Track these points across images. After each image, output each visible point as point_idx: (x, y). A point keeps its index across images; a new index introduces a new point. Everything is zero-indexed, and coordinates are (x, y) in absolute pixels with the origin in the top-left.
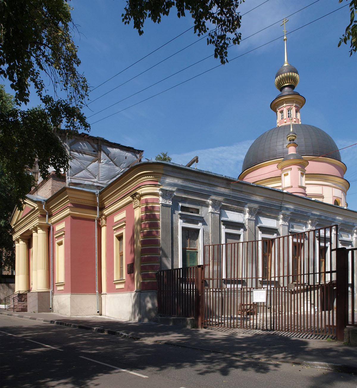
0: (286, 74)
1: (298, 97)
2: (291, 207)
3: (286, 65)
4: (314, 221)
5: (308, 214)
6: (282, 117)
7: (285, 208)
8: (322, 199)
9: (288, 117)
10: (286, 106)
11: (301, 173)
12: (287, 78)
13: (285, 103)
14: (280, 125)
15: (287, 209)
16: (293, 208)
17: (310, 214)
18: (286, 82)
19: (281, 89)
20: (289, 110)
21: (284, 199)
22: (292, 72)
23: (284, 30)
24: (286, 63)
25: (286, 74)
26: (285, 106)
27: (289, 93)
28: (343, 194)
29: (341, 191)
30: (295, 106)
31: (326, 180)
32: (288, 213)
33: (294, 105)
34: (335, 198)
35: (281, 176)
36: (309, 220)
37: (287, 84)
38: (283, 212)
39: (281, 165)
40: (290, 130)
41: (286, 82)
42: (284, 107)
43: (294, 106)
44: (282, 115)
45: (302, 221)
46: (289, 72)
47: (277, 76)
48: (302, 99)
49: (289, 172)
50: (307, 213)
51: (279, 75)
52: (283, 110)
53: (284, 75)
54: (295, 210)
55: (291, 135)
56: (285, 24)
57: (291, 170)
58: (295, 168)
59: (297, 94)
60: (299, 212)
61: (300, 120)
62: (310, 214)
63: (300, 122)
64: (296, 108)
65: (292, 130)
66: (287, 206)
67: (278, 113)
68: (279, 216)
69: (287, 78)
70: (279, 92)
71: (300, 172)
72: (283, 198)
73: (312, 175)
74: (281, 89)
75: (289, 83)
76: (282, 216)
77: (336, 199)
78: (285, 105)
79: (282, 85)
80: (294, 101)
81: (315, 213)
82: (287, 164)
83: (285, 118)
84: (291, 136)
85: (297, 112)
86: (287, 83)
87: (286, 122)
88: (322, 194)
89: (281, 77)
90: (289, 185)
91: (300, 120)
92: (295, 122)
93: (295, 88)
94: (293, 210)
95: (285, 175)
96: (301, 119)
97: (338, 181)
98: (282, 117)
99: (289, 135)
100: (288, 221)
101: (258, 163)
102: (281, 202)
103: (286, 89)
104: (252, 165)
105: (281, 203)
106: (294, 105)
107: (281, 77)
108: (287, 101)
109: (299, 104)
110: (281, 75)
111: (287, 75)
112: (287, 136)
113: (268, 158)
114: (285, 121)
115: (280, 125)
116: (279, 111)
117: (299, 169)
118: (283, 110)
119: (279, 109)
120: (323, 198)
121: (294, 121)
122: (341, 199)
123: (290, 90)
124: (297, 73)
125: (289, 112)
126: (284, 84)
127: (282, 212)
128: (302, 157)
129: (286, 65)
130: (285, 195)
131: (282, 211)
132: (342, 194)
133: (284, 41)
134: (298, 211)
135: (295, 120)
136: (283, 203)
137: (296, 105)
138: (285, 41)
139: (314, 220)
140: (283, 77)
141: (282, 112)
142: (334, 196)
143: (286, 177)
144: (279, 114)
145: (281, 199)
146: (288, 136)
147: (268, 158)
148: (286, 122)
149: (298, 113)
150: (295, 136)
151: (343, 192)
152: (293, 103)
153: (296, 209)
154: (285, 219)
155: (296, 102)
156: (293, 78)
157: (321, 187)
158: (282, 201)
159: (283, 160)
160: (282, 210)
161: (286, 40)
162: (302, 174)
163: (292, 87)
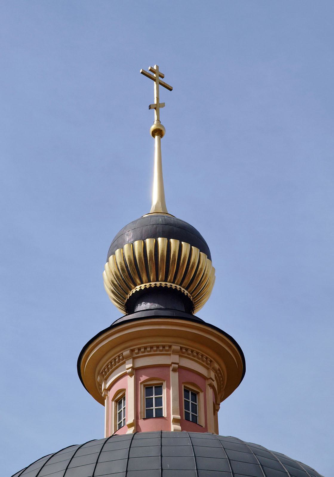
80: (170, 347)
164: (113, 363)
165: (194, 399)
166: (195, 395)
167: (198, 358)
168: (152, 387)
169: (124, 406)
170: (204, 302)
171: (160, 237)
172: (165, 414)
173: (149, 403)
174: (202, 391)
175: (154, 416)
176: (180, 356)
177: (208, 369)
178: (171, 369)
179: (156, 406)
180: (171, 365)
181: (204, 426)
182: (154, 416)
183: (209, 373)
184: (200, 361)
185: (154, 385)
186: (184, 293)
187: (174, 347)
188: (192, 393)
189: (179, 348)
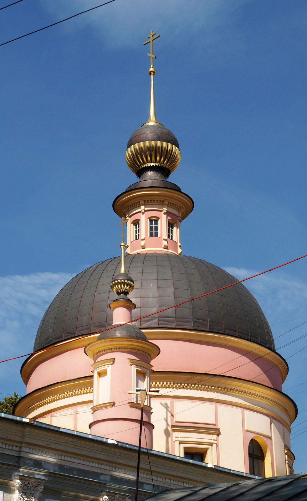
0: (147, 143)
1: (172, 194)
2: (51, 459)
3: (151, 124)
4: (118, 496)
5: (102, 477)
6: (136, 233)
7: (31, 463)
8: (215, 437)
9: (149, 235)
10: (146, 211)
11: (137, 371)
12: (150, 151)
13: (143, 205)
14: (132, 251)
15: (38, 464)
16: (55, 461)
17: (108, 478)
18: (149, 159)
19: (140, 172)
20: (154, 220)
21: (27, 440)
22: (167, 142)
23: (150, 53)
24: (152, 121)
25: (147, 143)
26: (143, 211)
27: (153, 183)
28: (274, 424)
29: (267, 419)
30: (167, 213)
31: (226, 390)
32: (40, 474)
33: (165, 209)
34: (251, 436)
35: (93, 376)
36: (103, 493)
37: (152, 164)
38: (23, 472)
39: (94, 348)
40: (120, 271)
41: (149, 159)
42: (140, 212)
43: (165, 213)
44: (136, 231)
45: (82, 495)
46: (156, 140)
47: (129, 146)
48: (187, 201)
49: (109, 368)
50: (97, 475)
51: (134, 144)
52: (139, 220)
53: (144, 146)
54: (61, 467)
55: (119, 281)
56: (152, 43)
57: (114, 362)
58: (122, 358)
59: (178, 190)
60: (75, 472)
61: (179, 244)
62: (108, 478)
63: (179, 248)
64: (169, 218)
65: (125, 271)
66: (36, 457)
67: (129, 223)
68: (12, 482)
69: (150, 151)
70: (133, 178)
71: (134, 369)
72: (23, 437)
73: (189, 377)
74: (140, 172)
75: (156, 162)
76: (18, 481)
77: (255, 437)
78: (143, 208)
79: (141, 164)
80: (163, 201)
81: (122, 475)
82: (103, 348)
83: (143, 237)
84: (121, 283)
85: (171, 225)
86: (151, 162)
87: (143, 247)
88: (215, 425)
89: (138, 149)
90: (108, 400)
91: (179, 244)
92: (166, 248)
93: (171, 174)
94: (56, 468)
95: (100, 374)
96: (180, 242)
97: (259, 394)
98: (138, 234)
99: (116, 281)
100: (38, 494)
101: (64, 338)
102: (20, 445)
103: (150, 174)
104: (52, 341)
105: (20, 447)
106: (165, 209)
107: (138, 149)
108: (148, 201)
109: (178, 208)
110: (137, 145)
111: (156, 145)
112: (112, 282)
113: (87, 329)
114: (143, 243)
115: (132, 251)
116: (130, 220)
117: (133, 362)
118: (139, 220)
119: (130, 217)
120: (218, 435)
121: (163, 246)
122: (270, 438)
123: (158, 178)
124: (175, 142)
125: (154, 225)
126: (144, 163)
127: (20, 471)
128: (143, 331)
129: (151, 124)
130: (28, 429)
131: (21, 469)
132: (272, 425)
133: (150, 74)
134: (71, 470)
135: (165, 243)
136: (24, 449)
137: (169, 211)
138: (152, 76)
139: (116, 494)
140: (141, 149)
141: (136, 223)
142: (247, 431)
143: (102, 379)
144: (131, 229)
145: (18, 439)
146: (114, 283)
147: (87, 329)
148: (143, 247)
149: (175, 229)
150: (128, 284)
151: (274, 420)
152: (161, 206)
153: (64, 463)
154: (28, 488)
155: (169, 205)
156: (164, 153)
157: (211, 406)
158: (21, 443)
159: (99, 339)
160: (20, 467)
161: (154, 75)
162: (141, 375)
163: (164, 171)
164: (131, 206)
165: (156, 223)
166: (156, 222)
167: (173, 206)
168: (153, 220)
169: (137, 230)
170: (159, 150)
171: (159, 141)
172: (159, 235)
173: (151, 228)
174: (175, 223)
175: (154, 236)
176: (168, 206)
177: (179, 211)
178: (163, 212)
179: (155, 230)
180: (163, 211)
181: (176, 242)
182: (154, 236)
183: (179, 214)
184: (172, 207)
185: (154, 219)
186: (165, 167)
187: (165, 202)
188: (171, 224)
189: (167, 203)
